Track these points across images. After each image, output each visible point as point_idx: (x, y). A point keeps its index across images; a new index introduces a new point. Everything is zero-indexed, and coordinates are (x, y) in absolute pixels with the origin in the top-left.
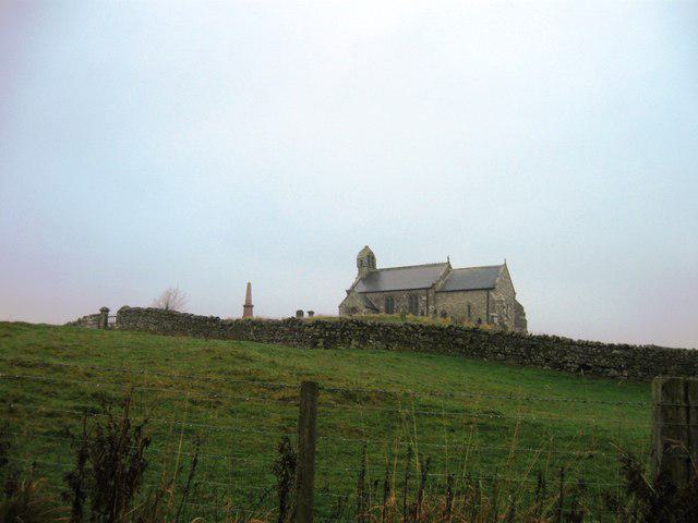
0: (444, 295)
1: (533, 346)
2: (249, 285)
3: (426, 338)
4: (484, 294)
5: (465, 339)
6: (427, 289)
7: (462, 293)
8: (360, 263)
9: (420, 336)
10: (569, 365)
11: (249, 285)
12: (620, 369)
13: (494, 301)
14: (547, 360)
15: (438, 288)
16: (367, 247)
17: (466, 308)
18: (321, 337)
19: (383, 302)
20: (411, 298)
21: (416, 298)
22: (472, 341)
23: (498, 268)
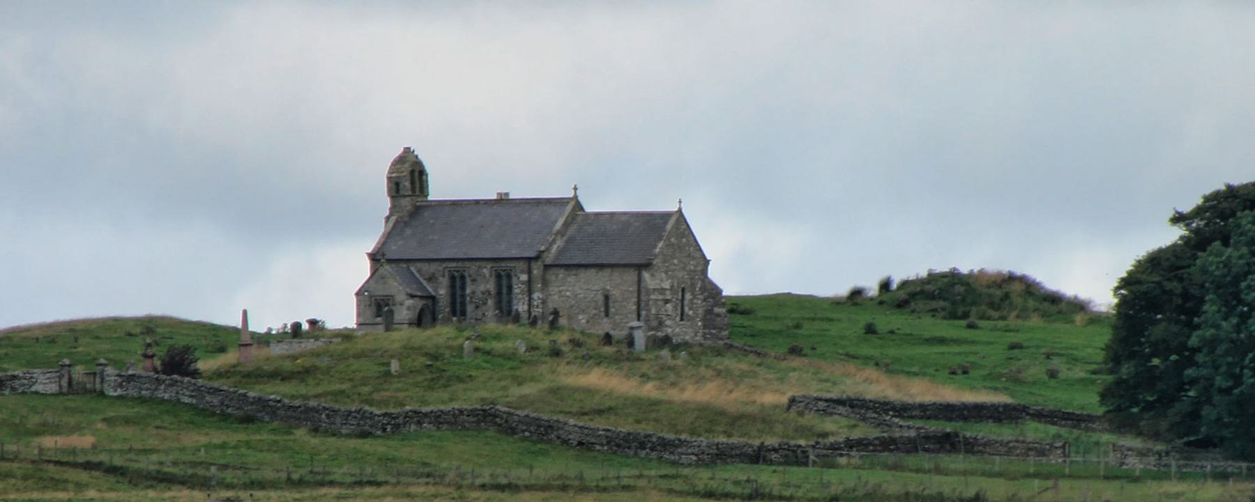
0: (561, 273)
1: (550, 426)
2: (245, 313)
3: (471, 419)
4: (631, 276)
5: (502, 418)
6: (529, 259)
7: (592, 271)
8: (395, 188)
9: (466, 418)
10: (571, 441)
11: (245, 313)
12: (602, 445)
13: (648, 292)
14: (558, 438)
15: (549, 258)
16: (407, 151)
17: (600, 298)
18: (389, 424)
19: (445, 281)
20: (499, 277)
21: (509, 277)
22: (506, 421)
23: (666, 216)
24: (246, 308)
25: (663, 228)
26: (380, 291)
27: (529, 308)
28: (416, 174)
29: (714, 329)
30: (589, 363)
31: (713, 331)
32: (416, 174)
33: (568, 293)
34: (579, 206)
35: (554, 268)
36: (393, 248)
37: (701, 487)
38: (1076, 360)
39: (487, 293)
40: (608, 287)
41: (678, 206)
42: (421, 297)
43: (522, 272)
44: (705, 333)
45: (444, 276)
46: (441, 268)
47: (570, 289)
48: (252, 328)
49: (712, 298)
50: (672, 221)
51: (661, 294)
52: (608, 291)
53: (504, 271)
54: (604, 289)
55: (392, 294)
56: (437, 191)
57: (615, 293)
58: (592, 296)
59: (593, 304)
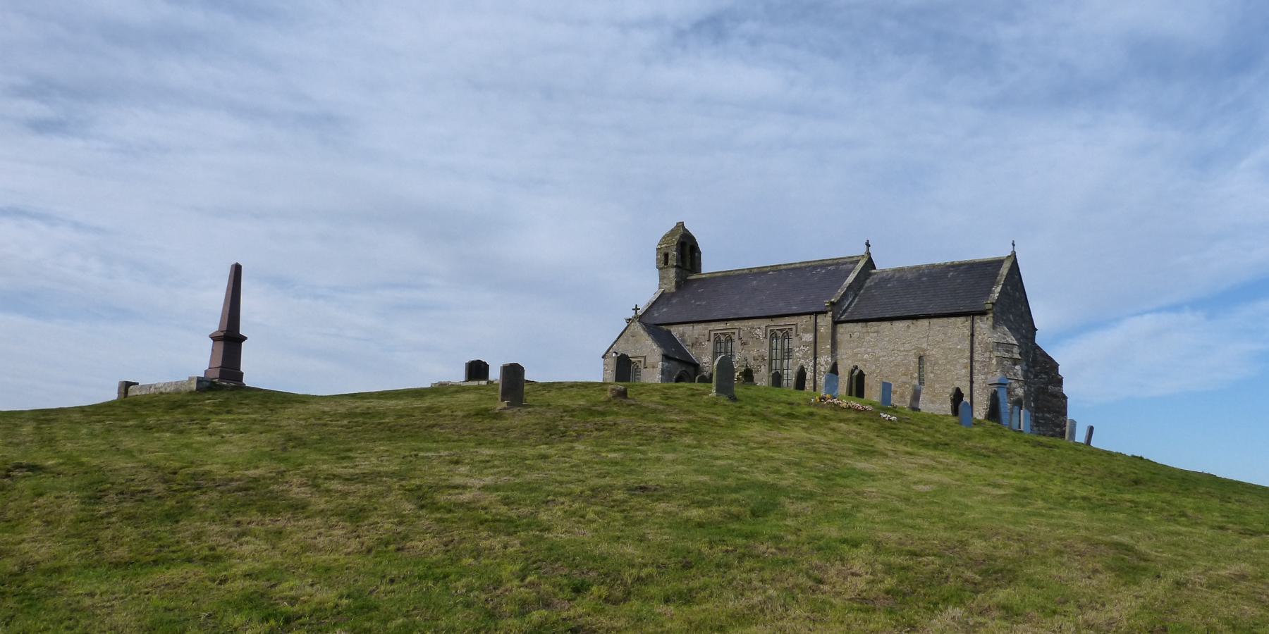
11: (1091, 429)
17: (914, 361)
23: (998, 263)
24: (1092, 425)
25: (996, 275)
26: (623, 349)
27: (815, 376)
28: (688, 248)
29: (1049, 413)
30: (934, 471)
31: (1048, 415)
32: (688, 248)
33: (866, 356)
34: (870, 264)
35: (713, 323)
36: (656, 315)
37: (224, 618)
38: (1077, 450)
39: (760, 359)
40: (925, 346)
41: (1012, 250)
42: (679, 361)
43: (805, 331)
44: (1036, 417)
45: (709, 341)
46: (707, 332)
47: (869, 350)
48: (1095, 443)
49: (1046, 373)
50: (1004, 270)
51: (1008, 351)
52: (924, 350)
53: (781, 330)
54: (917, 348)
55: (851, 367)
56: (709, 265)
57: (934, 352)
58: (899, 359)
59: (902, 369)
